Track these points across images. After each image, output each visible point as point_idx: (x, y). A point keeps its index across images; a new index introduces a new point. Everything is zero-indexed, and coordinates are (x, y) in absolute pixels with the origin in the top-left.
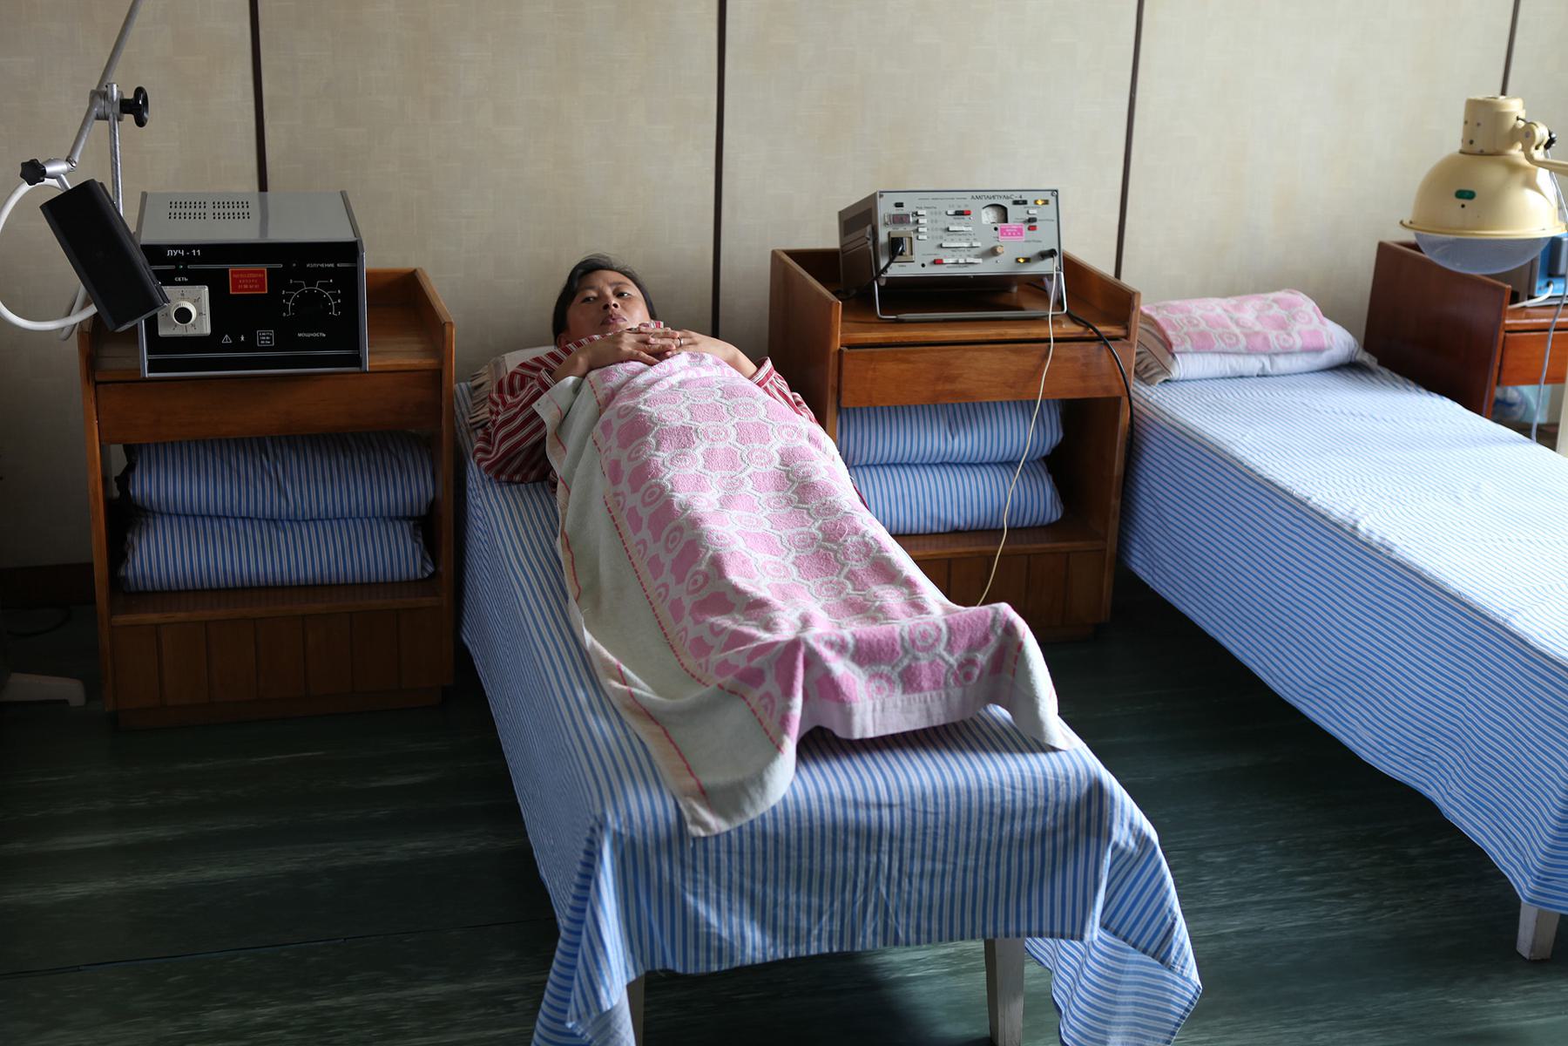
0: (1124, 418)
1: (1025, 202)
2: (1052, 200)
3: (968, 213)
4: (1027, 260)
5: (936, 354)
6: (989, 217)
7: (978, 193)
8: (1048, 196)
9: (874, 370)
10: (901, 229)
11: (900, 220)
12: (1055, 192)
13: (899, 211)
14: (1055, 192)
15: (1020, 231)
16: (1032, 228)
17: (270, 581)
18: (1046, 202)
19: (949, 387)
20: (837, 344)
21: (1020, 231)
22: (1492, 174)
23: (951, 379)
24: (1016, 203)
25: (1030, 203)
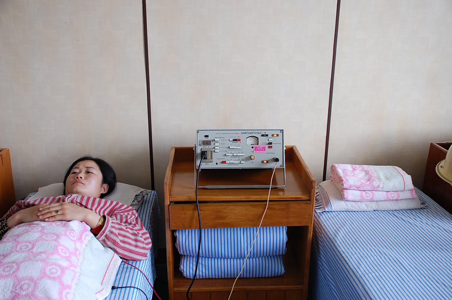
0: (310, 235)
1: (267, 135)
2: (280, 134)
3: (239, 140)
4: (267, 162)
5: (214, 207)
6: (250, 141)
7: (244, 132)
8: (278, 132)
9: (185, 214)
10: (207, 147)
11: (207, 143)
12: (282, 131)
13: (207, 139)
14: (282, 131)
15: (264, 149)
16: (271, 147)
17: (207, 276)
18: (278, 135)
19: (221, 221)
20: (167, 202)
21: (264, 149)
22: (341, 179)
23: (223, 218)
24: (263, 135)
25: (270, 136)
